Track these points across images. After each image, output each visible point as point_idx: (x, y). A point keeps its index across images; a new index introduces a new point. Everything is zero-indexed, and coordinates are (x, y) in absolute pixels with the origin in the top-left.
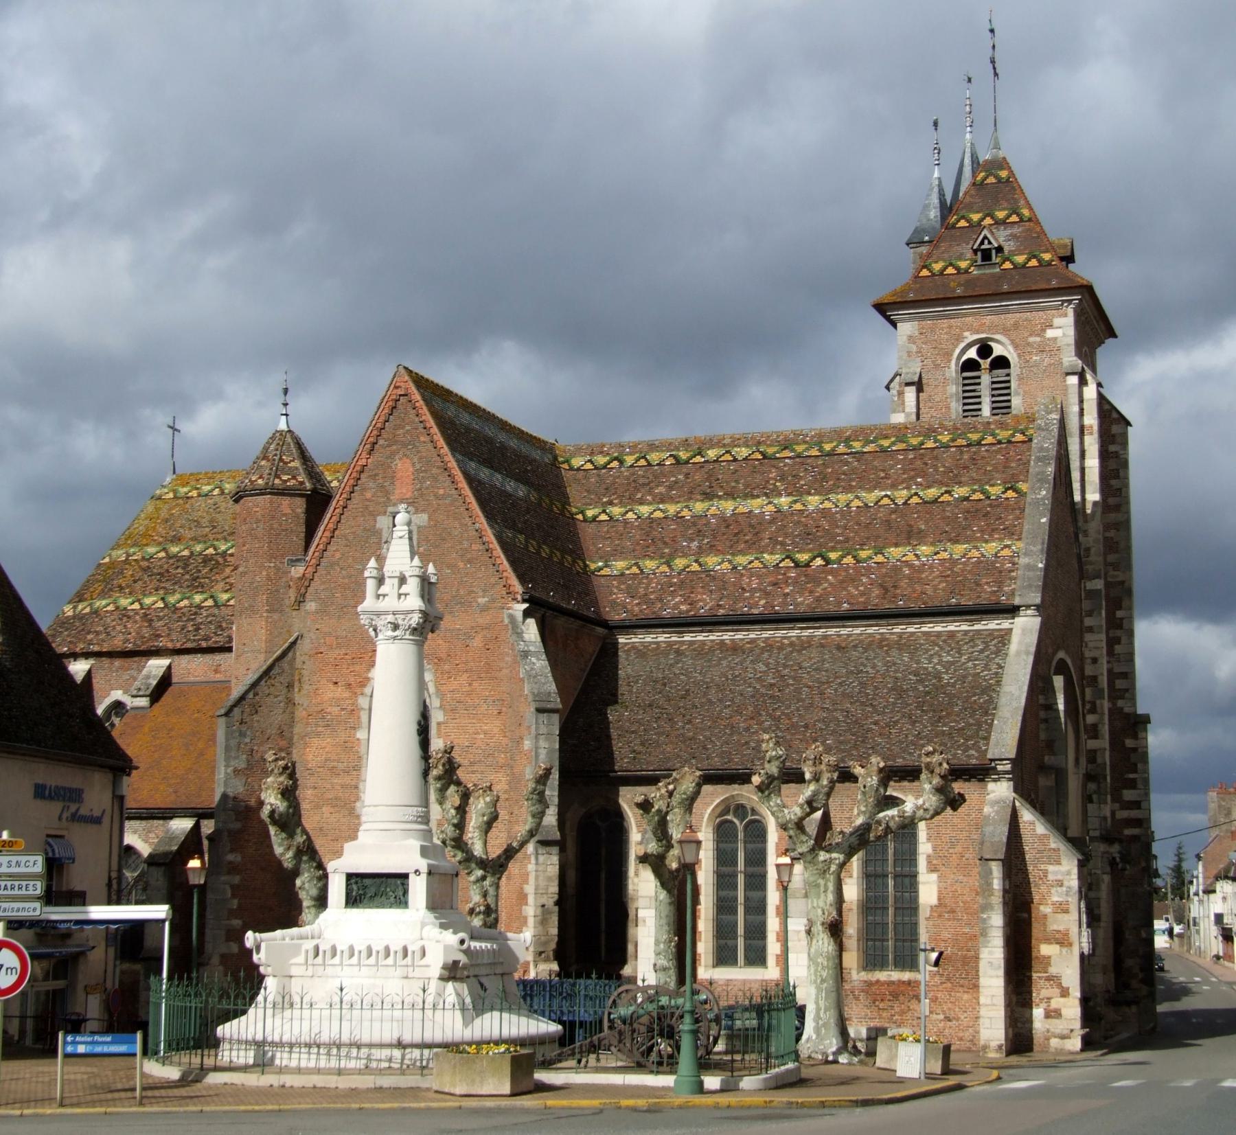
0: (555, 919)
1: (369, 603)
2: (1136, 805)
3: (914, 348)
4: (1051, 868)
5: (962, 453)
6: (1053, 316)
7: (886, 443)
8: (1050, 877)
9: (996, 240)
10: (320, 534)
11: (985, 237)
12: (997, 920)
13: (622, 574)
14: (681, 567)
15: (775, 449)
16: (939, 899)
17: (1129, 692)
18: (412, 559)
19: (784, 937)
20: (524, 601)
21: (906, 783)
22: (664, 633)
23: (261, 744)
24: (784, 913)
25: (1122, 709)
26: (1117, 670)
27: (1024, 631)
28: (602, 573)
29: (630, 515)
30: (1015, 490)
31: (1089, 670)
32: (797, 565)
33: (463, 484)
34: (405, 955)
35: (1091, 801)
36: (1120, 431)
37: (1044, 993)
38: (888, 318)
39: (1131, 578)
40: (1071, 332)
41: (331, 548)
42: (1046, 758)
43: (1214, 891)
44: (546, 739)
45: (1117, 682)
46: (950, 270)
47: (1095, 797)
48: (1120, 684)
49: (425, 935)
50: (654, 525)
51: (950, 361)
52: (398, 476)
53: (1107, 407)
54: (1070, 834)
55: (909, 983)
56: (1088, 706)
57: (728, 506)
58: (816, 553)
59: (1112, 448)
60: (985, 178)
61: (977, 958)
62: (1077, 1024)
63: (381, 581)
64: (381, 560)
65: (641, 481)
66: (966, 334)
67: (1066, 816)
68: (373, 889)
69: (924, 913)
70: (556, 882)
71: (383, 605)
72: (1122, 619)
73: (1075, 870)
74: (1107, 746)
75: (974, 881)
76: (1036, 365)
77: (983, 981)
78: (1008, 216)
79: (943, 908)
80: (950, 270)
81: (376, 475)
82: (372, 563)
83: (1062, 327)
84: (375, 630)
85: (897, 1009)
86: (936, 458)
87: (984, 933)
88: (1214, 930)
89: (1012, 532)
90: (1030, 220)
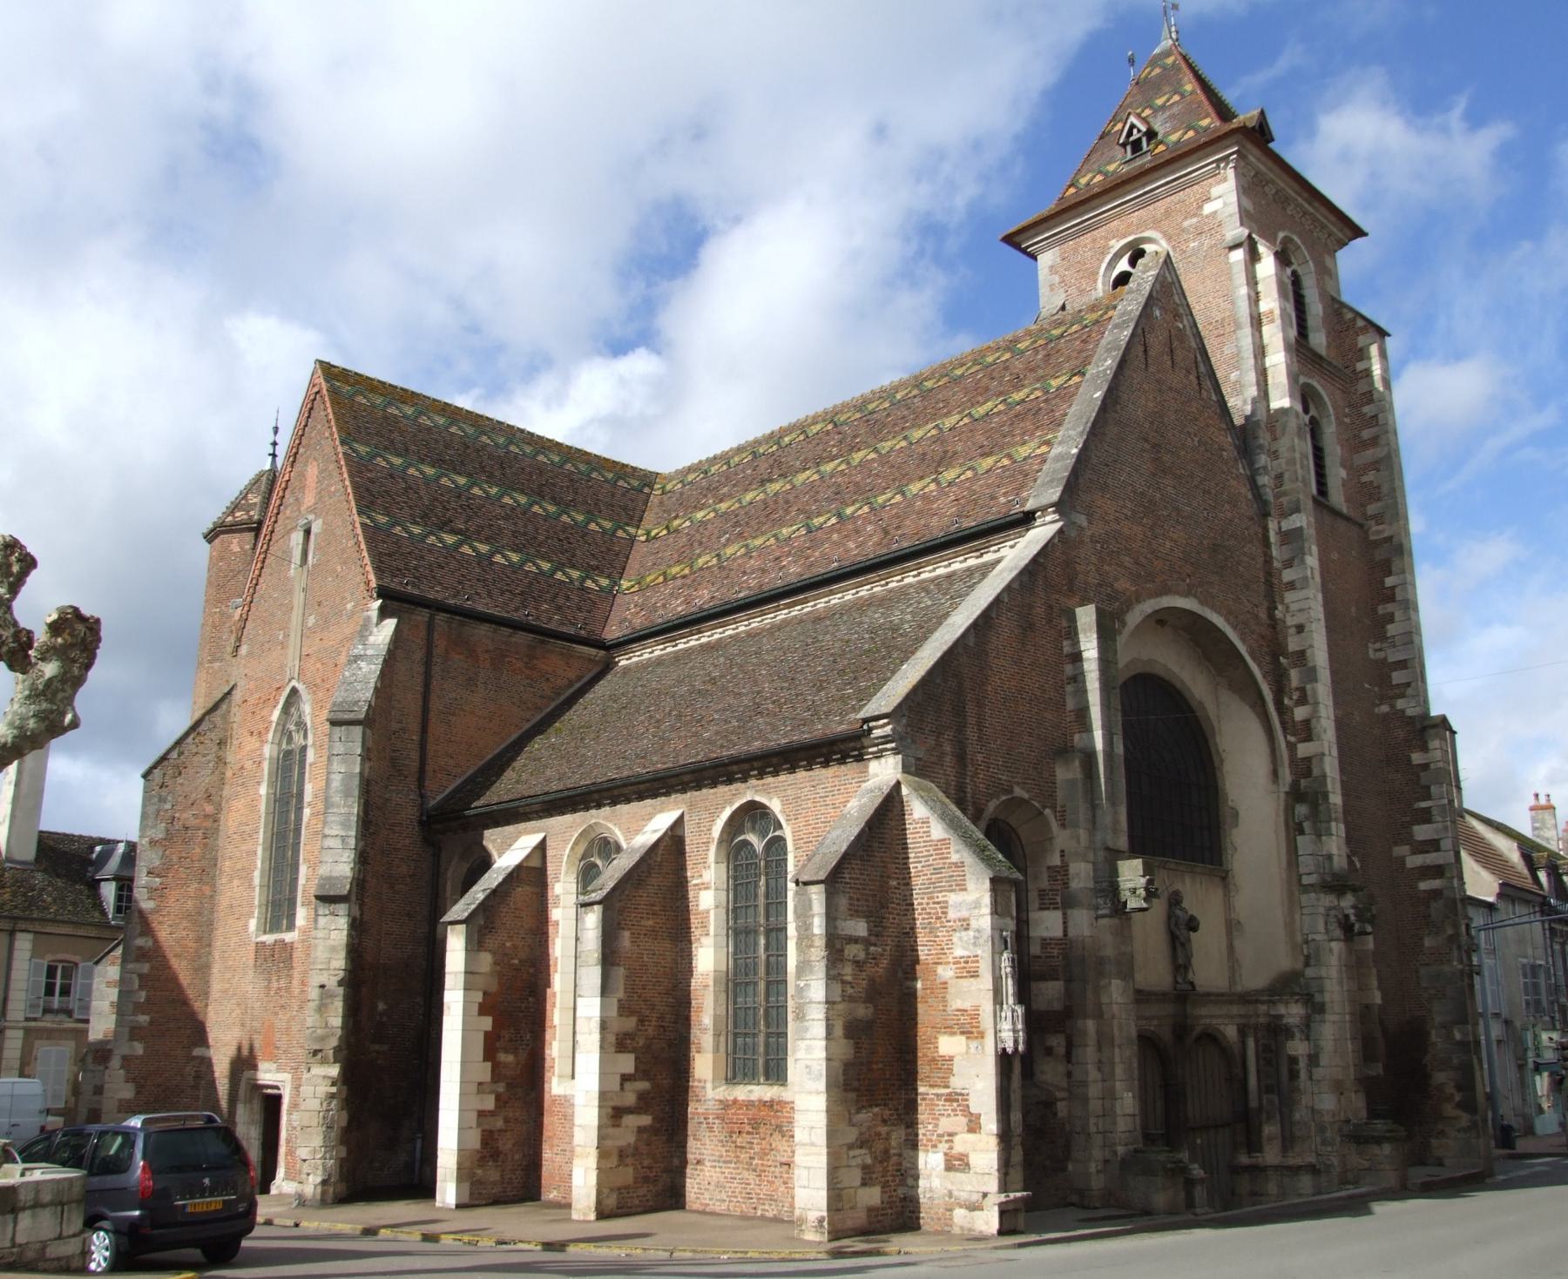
0: (338, 1006)
2: (1433, 845)
3: (1057, 279)
4: (953, 898)
6: (1211, 186)
8: (952, 914)
11: (1133, 126)
21: (770, 780)
23: (183, 810)
25: (1403, 711)
31: (1293, 644)
35: (1302, 832)
37: (945, 1124)
38: (1024, 251)
40: (1233, 198)
42: (1077, 737)
44: (344, 761)
47: (1306, 825)
51: (1095, 281)
62: (993, 1185)
66: (1112, 242)
72: (1393, 588)
73: (987, 899)
76: (1196, 251)
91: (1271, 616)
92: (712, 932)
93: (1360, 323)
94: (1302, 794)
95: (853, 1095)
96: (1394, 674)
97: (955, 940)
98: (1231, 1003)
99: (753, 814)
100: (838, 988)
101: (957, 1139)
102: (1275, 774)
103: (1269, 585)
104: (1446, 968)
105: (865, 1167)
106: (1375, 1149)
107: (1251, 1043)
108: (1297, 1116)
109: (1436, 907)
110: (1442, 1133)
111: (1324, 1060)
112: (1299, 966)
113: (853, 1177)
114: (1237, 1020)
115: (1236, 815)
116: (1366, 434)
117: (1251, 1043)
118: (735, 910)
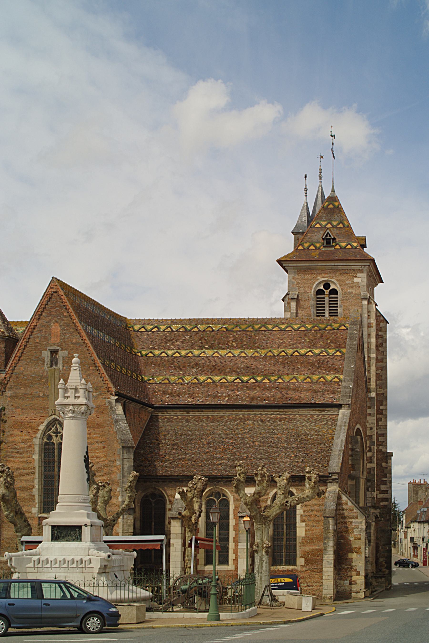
1: (60, 400)
4: (354, 520)
5: (317, 333)
7: (283, 327)
8: (353, 524)
10: (13, 358)
11: (328, 233)
12: (331, 543)
13: (160, 383)
15: (232, 327)
16: (306, 534)
17: (384, 443)
18: (81, 380)
19: (236, 552)
20: (116, 395)
22: (180, 411)
24: (236, 541)
25: (381, 450)
26: (379, 433)
27: (343, 414)
28: (150, 382)
29: (163, 355)
30: (340, 352)
32: (242, 382)
33: (85, 337)
34: (82, 563)
35: (368, 491)
36: (384, 326)
39: (386, 392)
40: (365, 280)
41: (19, 365)
42: (352, 472)
43: (410, 527)
44: (128, 461)
45: (380, 438)
46: (312, 247)
48: (380, 439)
49: (90, 553)
50: (175, 360)
52: (53, 331)
53: (378, 314)
54: (361, 505)
56: (368, 449)
57: (210, 352)
58: (251, 377)
59: (380, 333)
60: (328, 205)
61: (322, 559)
62: (363, 587)
63: (66, 390)
64: (66, 381)
65: (168, 338)
67: (359, 497)
68: (62, 533)
70: (132, 527)
71: (66, 401)
72: (382, 410)
75: (321, 526)
76: (350, 294)
77: (324, 569)
78: (338, 224)
79: (306, 538)
80: (312, 247)
81: (42, 330)
82: (62, 381)
83: (361, 279)
84: (63, 413)
86: (305, 335)
87: (325, 549)
88: (410, 544)
90: (348, 227)
93: (382, 318)
101: (353, 577)
104: (386, 528)
106: (380, 580)
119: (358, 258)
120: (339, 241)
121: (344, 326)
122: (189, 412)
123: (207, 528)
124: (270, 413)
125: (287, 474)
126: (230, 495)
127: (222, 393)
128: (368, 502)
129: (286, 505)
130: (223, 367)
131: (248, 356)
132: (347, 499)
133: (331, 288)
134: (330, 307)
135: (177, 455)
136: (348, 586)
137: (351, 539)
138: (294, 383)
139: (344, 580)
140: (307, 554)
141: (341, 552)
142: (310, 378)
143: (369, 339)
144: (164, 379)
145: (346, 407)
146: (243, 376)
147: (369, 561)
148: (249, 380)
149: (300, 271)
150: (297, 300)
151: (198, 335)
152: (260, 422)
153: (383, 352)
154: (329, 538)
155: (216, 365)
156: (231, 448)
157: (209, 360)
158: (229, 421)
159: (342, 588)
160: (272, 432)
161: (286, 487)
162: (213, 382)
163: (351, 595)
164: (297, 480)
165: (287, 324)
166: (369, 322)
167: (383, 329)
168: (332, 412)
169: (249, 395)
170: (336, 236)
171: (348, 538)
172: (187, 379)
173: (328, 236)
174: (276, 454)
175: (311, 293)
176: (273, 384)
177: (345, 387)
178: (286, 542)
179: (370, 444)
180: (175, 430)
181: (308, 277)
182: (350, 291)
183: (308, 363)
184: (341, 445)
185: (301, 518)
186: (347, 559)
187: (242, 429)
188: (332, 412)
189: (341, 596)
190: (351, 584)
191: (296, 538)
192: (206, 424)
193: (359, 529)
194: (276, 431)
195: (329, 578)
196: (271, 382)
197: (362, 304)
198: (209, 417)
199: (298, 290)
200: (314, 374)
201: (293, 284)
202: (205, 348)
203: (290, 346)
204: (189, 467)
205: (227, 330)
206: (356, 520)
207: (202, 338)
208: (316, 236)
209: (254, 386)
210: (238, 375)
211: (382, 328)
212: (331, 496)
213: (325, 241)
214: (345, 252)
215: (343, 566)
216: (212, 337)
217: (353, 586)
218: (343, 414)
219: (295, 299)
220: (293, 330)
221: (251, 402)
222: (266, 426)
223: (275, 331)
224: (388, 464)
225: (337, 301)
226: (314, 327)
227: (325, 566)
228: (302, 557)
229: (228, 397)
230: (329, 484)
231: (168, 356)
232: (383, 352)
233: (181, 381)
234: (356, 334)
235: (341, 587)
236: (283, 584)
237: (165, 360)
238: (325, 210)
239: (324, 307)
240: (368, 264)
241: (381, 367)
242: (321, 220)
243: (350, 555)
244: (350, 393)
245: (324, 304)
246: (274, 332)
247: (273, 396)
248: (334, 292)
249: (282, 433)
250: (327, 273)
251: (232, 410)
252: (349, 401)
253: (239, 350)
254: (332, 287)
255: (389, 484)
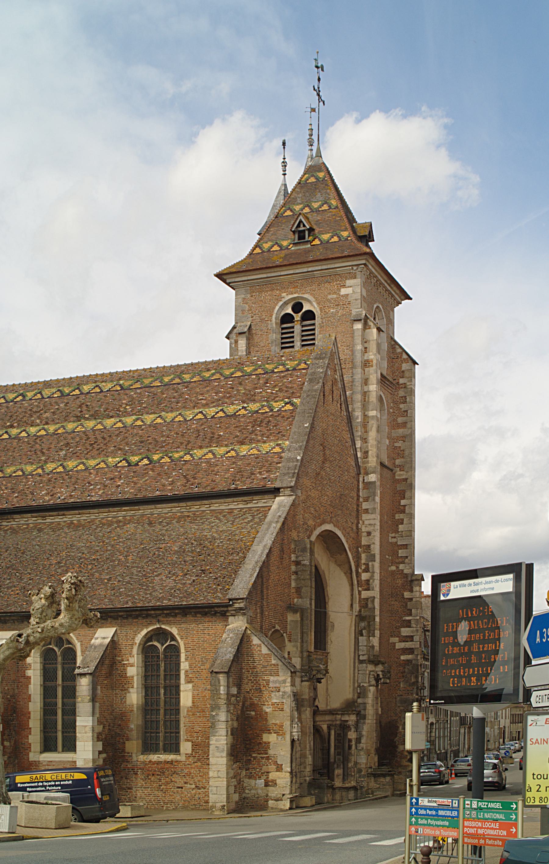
2: (410, 638)
4: (272, 678)
5: (259, 379)
7: (207, 375)
8: (271, 685)
9: (309, 222)
11: (301, 222)
13: (10, 476)
14: (51, 469)
15: (130, 382)
16: (193, 702)
25: (402, 570)
31: (364, 542)
35: (362, 635)
36: (407, 368)
42: (296, 600)
46: (276, 248)
55: (171, 762)
56: (363, 567)
57: (90, 424)
58: (144, 456)
69: (183, 713)
72: (405, 506)
74: (378, 596)
76: (333, 315)
77: (212, 760)
83: (353, 289)
85: (163, 781)
86: (240, 384)
87: (213, 726)
89: (281, 435)
91: (357, 526)
92: (135, 686)
94: (363, 620)
95: (232, 758)
96: (400, 551)
97: (272, 696)
98: (326, 714)
99: (162, 635)
100: (229, 715)
101: (270, 774)
102: (352, 605)
103: (358, 511)
105: (235, 786)
106: (382, 779)
107: (333, 732)
108: (350, 765)
109: (408, 668)
110: (400, 773)
111: (363, 741)
112: (356, 697)
113: (232, 789)
114: (327, 723)
115: (333, 626)
116: (400, 420)
117: (333, 732)
118: (145, 676)
119: (346, 253)
120: (319, 232)
121: (305, 363)
122: (45, 517)
123: (44, 694)
124: (166, 511)
125: (47, 588)
126: (76, 641)
127: (96, 484)
128: (360, 653)
129: (18, 641)
130: (104, 444)
131: (145, 424)
132: (260, 642)
133: (304, 310)
134: (303, 341)
135: (8, 581)
136: (262, 789)
137: (268, 710)
138: (208, 462)
139: (256, 779)
140: (195, 735)
141: (251, 732)
142: (235, 451)
143: (365, 387)
144: (18, 470)
145: (288, 492)
146: (132, 455)
147: (363, 748)
148: (140, 462)
149: (254, 288)
150: (249, 333)
151: (77, 402)
152: (146, 526)
153: (407, 411)
154: (219, 709)
155: (95, 442)
156: (90, 567)
157: (86, 435)
158: (101, 527)
159: (252, 791)
160: (161, 540)
161: (43, 611)
162: (87, 469)
163: (267, 804)
164: (178, 613)
165: (216, 369)
166: (366, 358)
167: (407, 374)
168: (264, 503)
169: (135, 483)
170: (316, 224)
171: (262, 709)
172: (50, 467)
173: (302, 226)
174: (155, 574)
175: (271, 321)
176: (175, 464)
177: (289, 460)
178: (165, 715)
179: (366, 559)
180: (17, 544)
181: (266, 296)
182: (334, 310)
183: (237, 427)
184: (262, 553)
185: (186, 676)
186: (260, 743)
187: (116, 538)
188: (264, 503)
189: (244, 804)
190: (266, 785)
191: (179, 709)
192: (66, 533)
193: (281, 693)
194: (166, 538)
195: (219, 775)
196: (172, 461)
197: (353, 330)
198: (73, 523)
199: (251, 319)
200: (242, 443)
201: (243, 311)
202: (85, 418)
203: (214, 402)
204: (19, 599)
205: (122, 388)
206: (276, 678)
207: (83, 404)
208: (283, 229)
209: (146, 469)
210: (125, 455)
211: (406, 372)
212: (231, 638)
213: (297, 236)
214: (327, 249)
215: (254, 755)
216: (98, 401)
217: (270, 788)
218: (280, 504)
219: (244, 333)
220: (222, 378)
221: (136, 495)
222: (154, 530)
223: (195, 382)
224: (414, 594)
225: (314, 330)
226: (257, 370)
227: (213, 754)
228: (188, 741)
229: (104, 489)
230: (231, 619)
231: (29, 435)
232: (407, 411)
233: (40, 471)
234: (322, 373)
235: (250, 790)
236: (71, 782)
237: (24, 442)
238: (302, 188)
239: (293, 342)
240: (364, 262)
241: (402, 437)
242: (294, 204)
243: (266, 737)
244: (295, 469)
245: (293, 337)
246: (192, 384)
247: (172, 483)
248: (310, 315)
249: (175, 541)
250: (297, 286)
251: (107, 510)
252: (291, 481)
253: (134, 417)
254: (306, 307)
255: (414, 626)
